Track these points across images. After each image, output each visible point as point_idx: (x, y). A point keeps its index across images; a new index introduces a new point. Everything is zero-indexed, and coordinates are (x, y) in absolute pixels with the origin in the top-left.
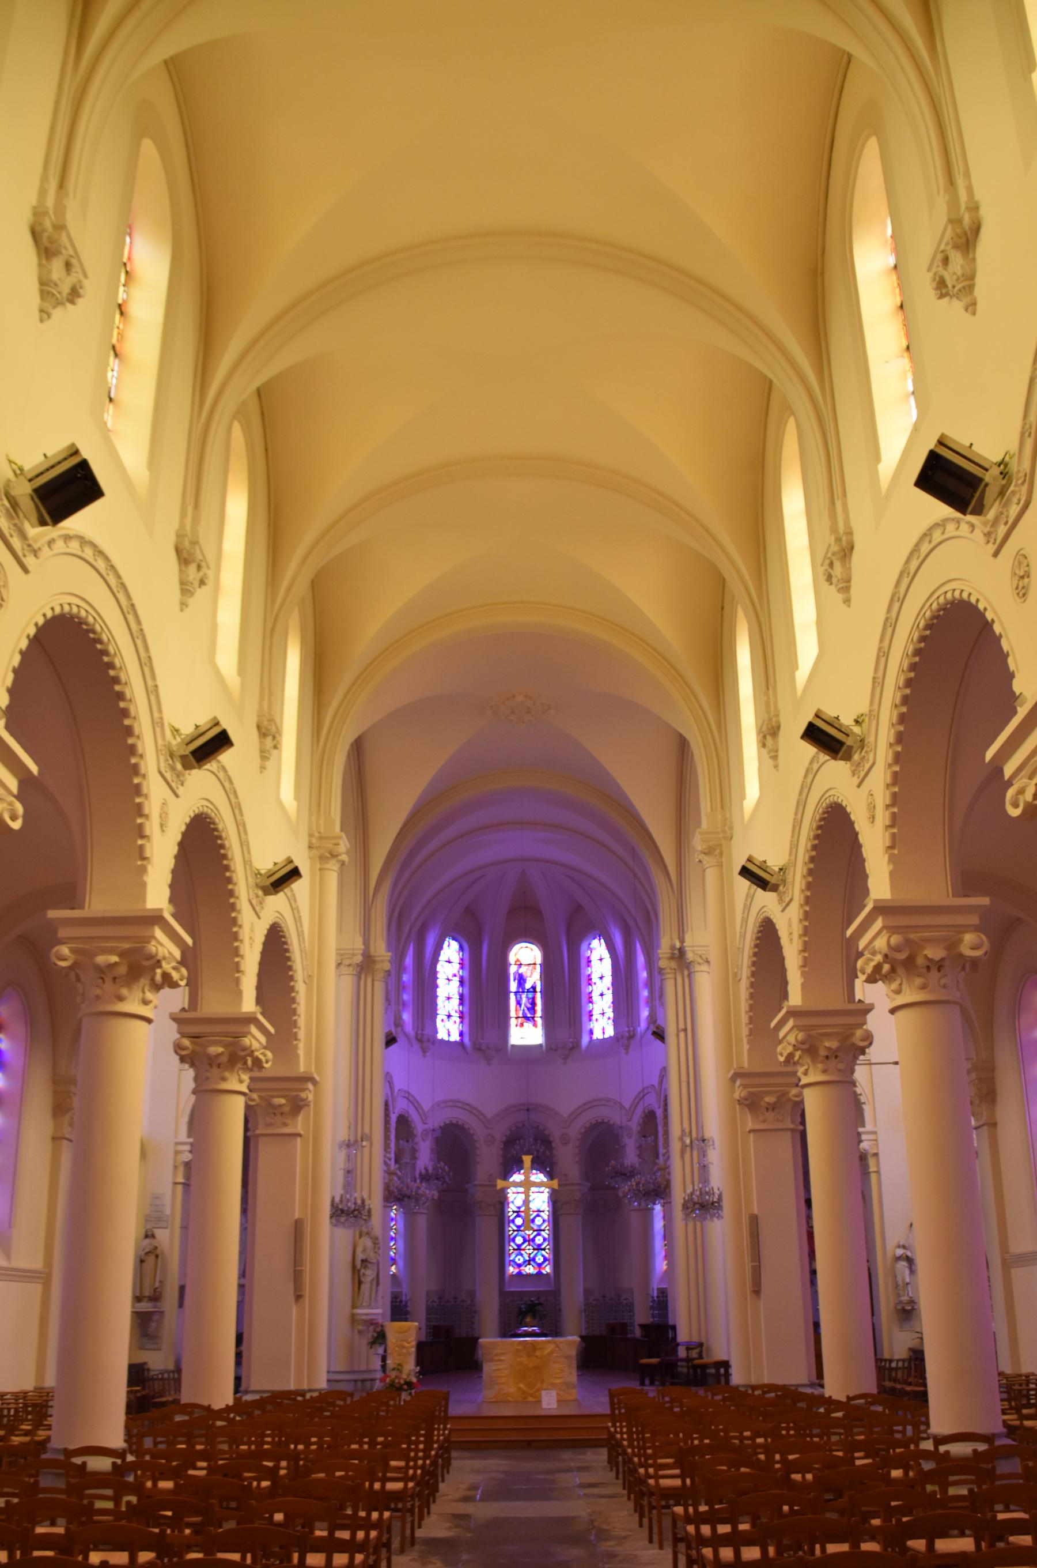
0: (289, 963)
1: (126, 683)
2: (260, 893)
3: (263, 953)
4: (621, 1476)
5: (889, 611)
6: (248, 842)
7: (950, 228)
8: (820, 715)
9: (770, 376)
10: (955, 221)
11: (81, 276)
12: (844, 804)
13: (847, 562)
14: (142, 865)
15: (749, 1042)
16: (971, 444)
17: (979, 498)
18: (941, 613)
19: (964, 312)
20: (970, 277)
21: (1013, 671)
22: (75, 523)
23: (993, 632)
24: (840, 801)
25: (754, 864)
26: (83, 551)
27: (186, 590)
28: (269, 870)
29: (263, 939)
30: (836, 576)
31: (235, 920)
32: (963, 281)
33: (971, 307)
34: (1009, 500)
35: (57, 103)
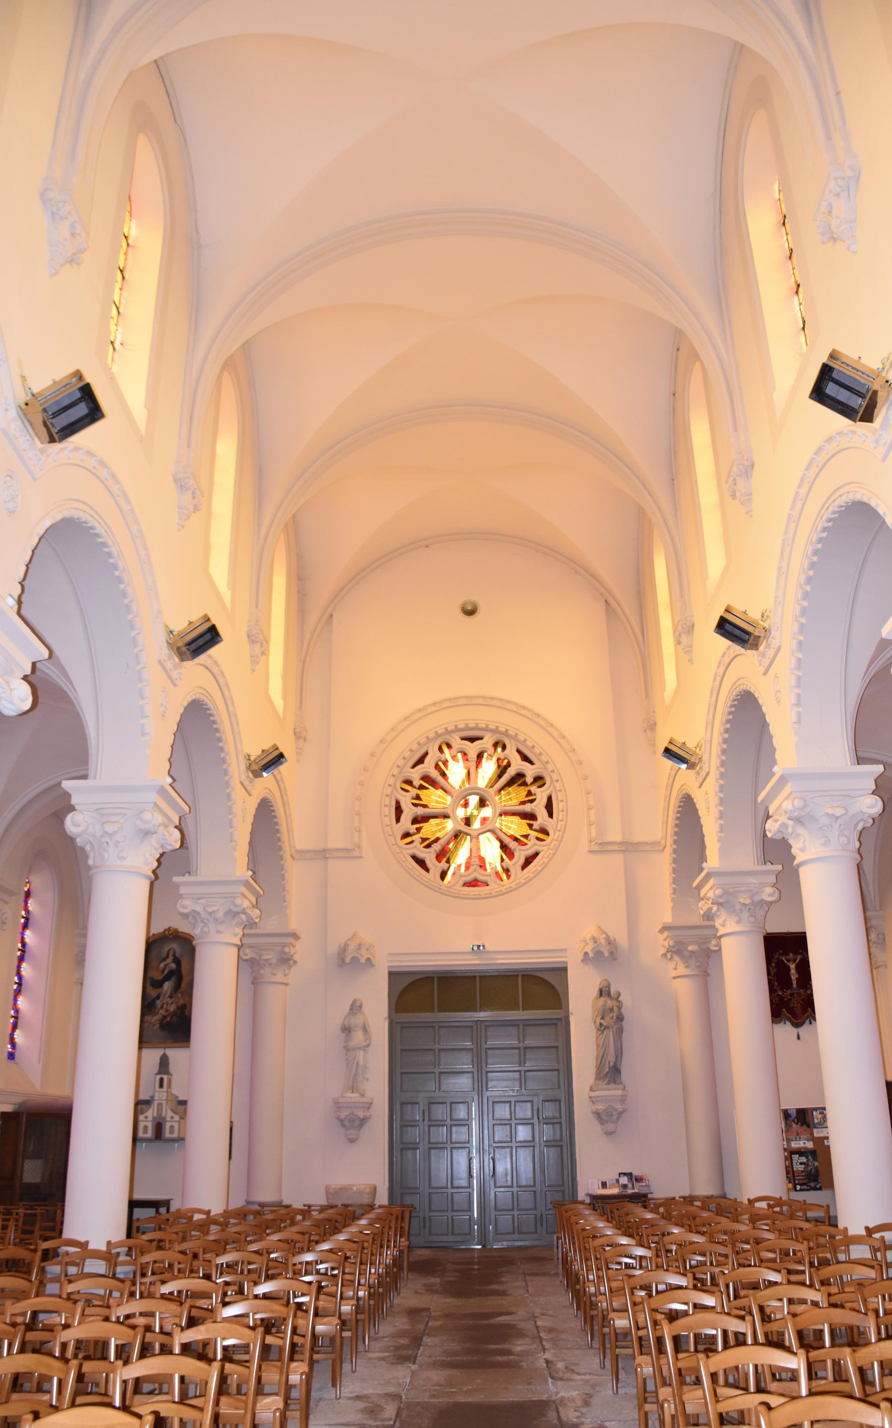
2: (251, 775)
6: (240, 732)
12: (752, 692)
24: (748, 689)
29: (254, 812)
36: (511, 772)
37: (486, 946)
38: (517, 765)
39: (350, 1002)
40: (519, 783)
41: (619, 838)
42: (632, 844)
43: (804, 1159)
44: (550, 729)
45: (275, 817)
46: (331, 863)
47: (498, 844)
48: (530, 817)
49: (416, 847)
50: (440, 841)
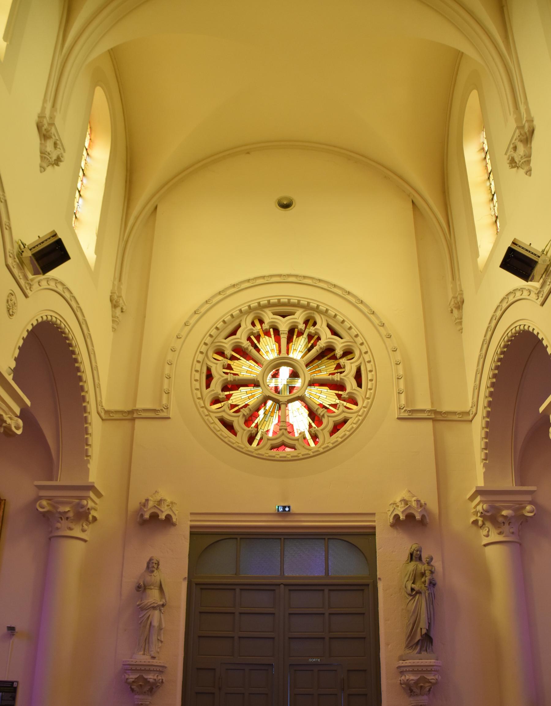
7: (517, 131)
8: (516, 243)
10: (520, 127)
11: (62, 151)
14: (87, 459)
16: (531, 244)
18: (509, 343)
20: (528, 157)
22: (54, 273)
23: (543, 345)
32: (525, 158)
33: (529, 172)
35: (118, 250)
36: (322, 344)
37: (291, 508)
38: (326, 337)
39: (148, 559)
40: (329, 356)
41: (428, 407)
42: (440, 413)
44: (360, 306)
46: (138, 424)
47: (306, 412)
48: (338, 386)
49: (224, 411)
50: (237, 376)
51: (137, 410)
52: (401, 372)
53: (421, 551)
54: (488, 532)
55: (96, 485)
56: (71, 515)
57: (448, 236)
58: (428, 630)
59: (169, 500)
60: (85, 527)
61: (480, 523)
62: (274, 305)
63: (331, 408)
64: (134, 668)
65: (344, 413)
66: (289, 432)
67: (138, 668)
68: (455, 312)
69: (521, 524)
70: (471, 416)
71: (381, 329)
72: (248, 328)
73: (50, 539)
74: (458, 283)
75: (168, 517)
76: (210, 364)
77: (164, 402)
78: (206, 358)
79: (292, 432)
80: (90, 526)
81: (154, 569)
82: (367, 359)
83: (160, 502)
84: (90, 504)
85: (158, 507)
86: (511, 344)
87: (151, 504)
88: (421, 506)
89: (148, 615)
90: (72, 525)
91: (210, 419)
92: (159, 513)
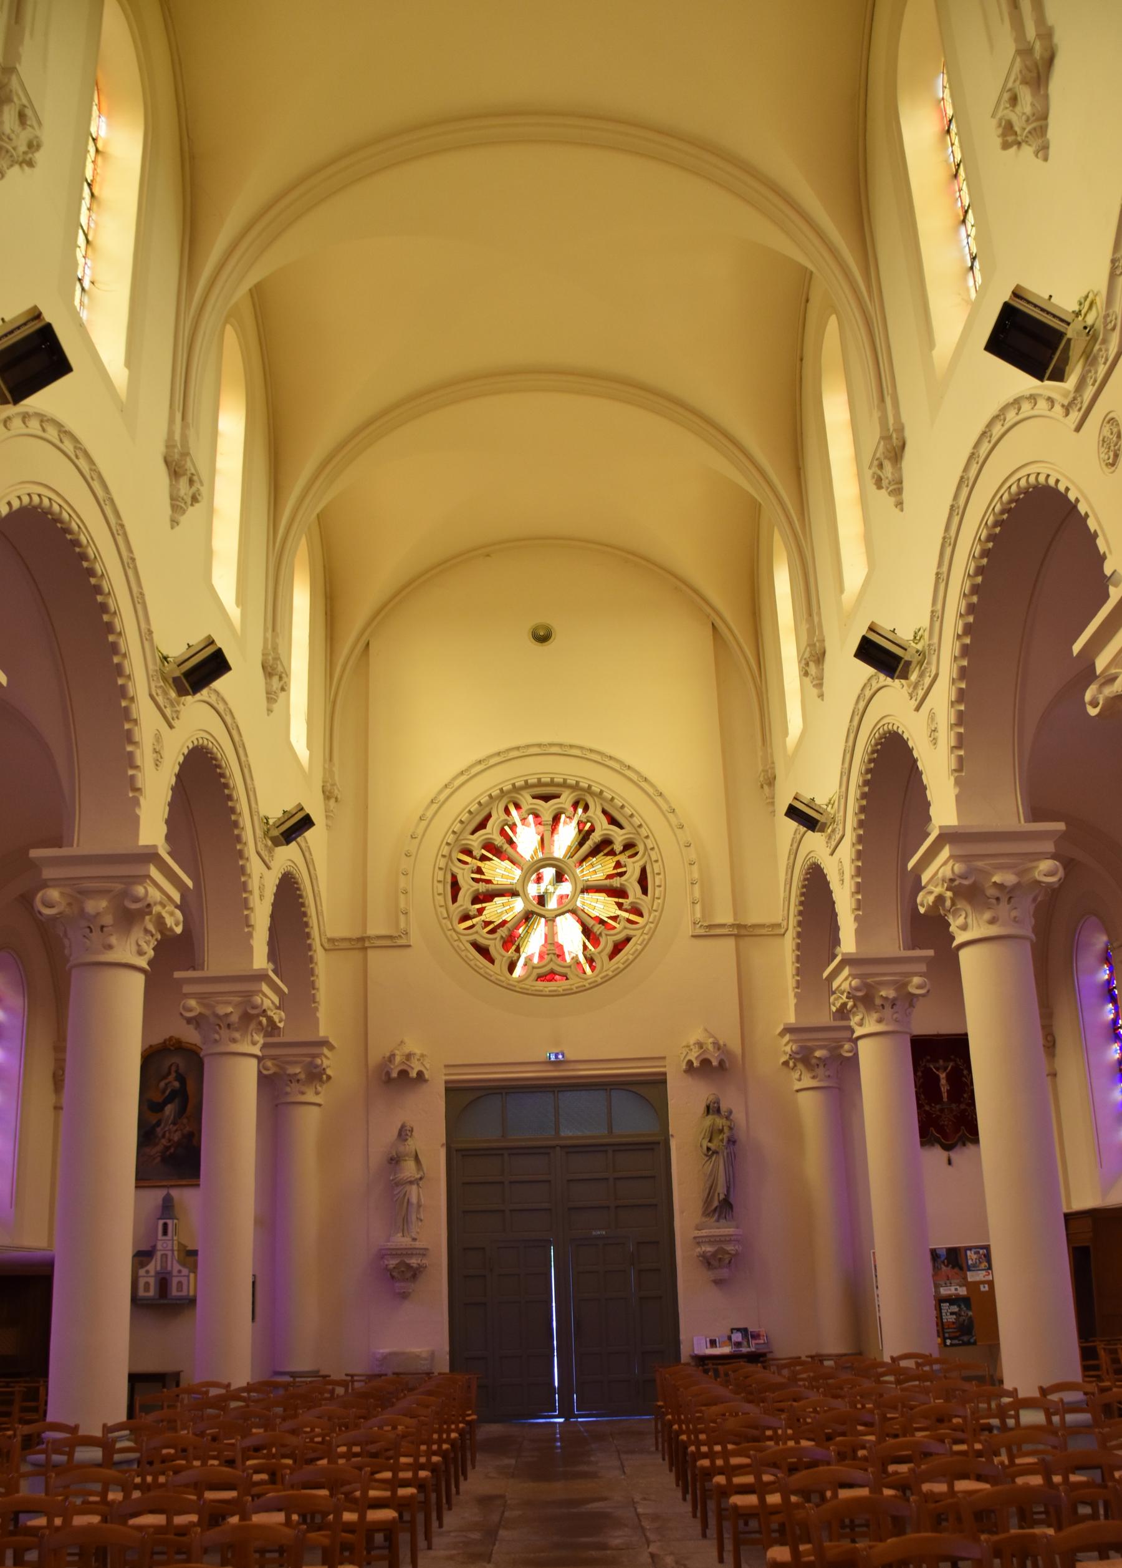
0: (305, 919)
1: (115, 613)
3: (275, 905)
4: (667, 1458)
5: (956, 497)
7: (1018, 60)
9: (810, 266)
10: (886, 437)
13: (898, 463)
14: (133, 797)
15: (796, 995)
16: (1051, 296)
17: (1064, 348)
18: (1013, 505)
19: (1035, 158)
20: (1041, 120)
21: (1104, 553)
22: (37, 401)
25: (801, 802)
26: (44, 430)
27: (177, 506)
28: (279, 819)
30: (887, 478)
31: (243, 868)
33: (1043, 151)
34: (1095, 359)
36: (596, 837)
37: (566, 1052)
40: (605, 851)
41: (729, 919)
43: (955, 1309)
45: (226, 786)
47: (579, 928)
48: (618, 893)
49: (477, 932)
51: (369, 938)
52: (696, 876)
53: (718, 1103)
54: (800, 1075)
55: (331, 1040)
56: (302, 1076)
57: (758, 679)
58: (727, 1196)
59: (418, 1051)
60: (319, 1088)
61: (791, 1064)
62: (533, 786)
63: (610, 921)
64: (394, 1252)
65: (626, 930)
66: (558, 956)
67: (399, 1252)
68: (766, 787)
69: (841, 1064)
70: (783, 931)
71: (671, 816)
72: (502, 819)
73: (277, 1106)
74: (769, 751)
75: (420, 1074)
76: (455, 870)
77: (402, 925)
78: (450, 863)
79: (561, 955)
80: (325, 1086)
81: (407, 1137)
82: (654, 858)
83: (409, 1056)
84: (326, 1063)
85: (408, 1063)
86: (1008, 518)
87: (398, 1059)
88: (719, 1049)
89: (404, 1192)
90: (304, 1089)
91: (461, 945)
92: (409, 1070)
